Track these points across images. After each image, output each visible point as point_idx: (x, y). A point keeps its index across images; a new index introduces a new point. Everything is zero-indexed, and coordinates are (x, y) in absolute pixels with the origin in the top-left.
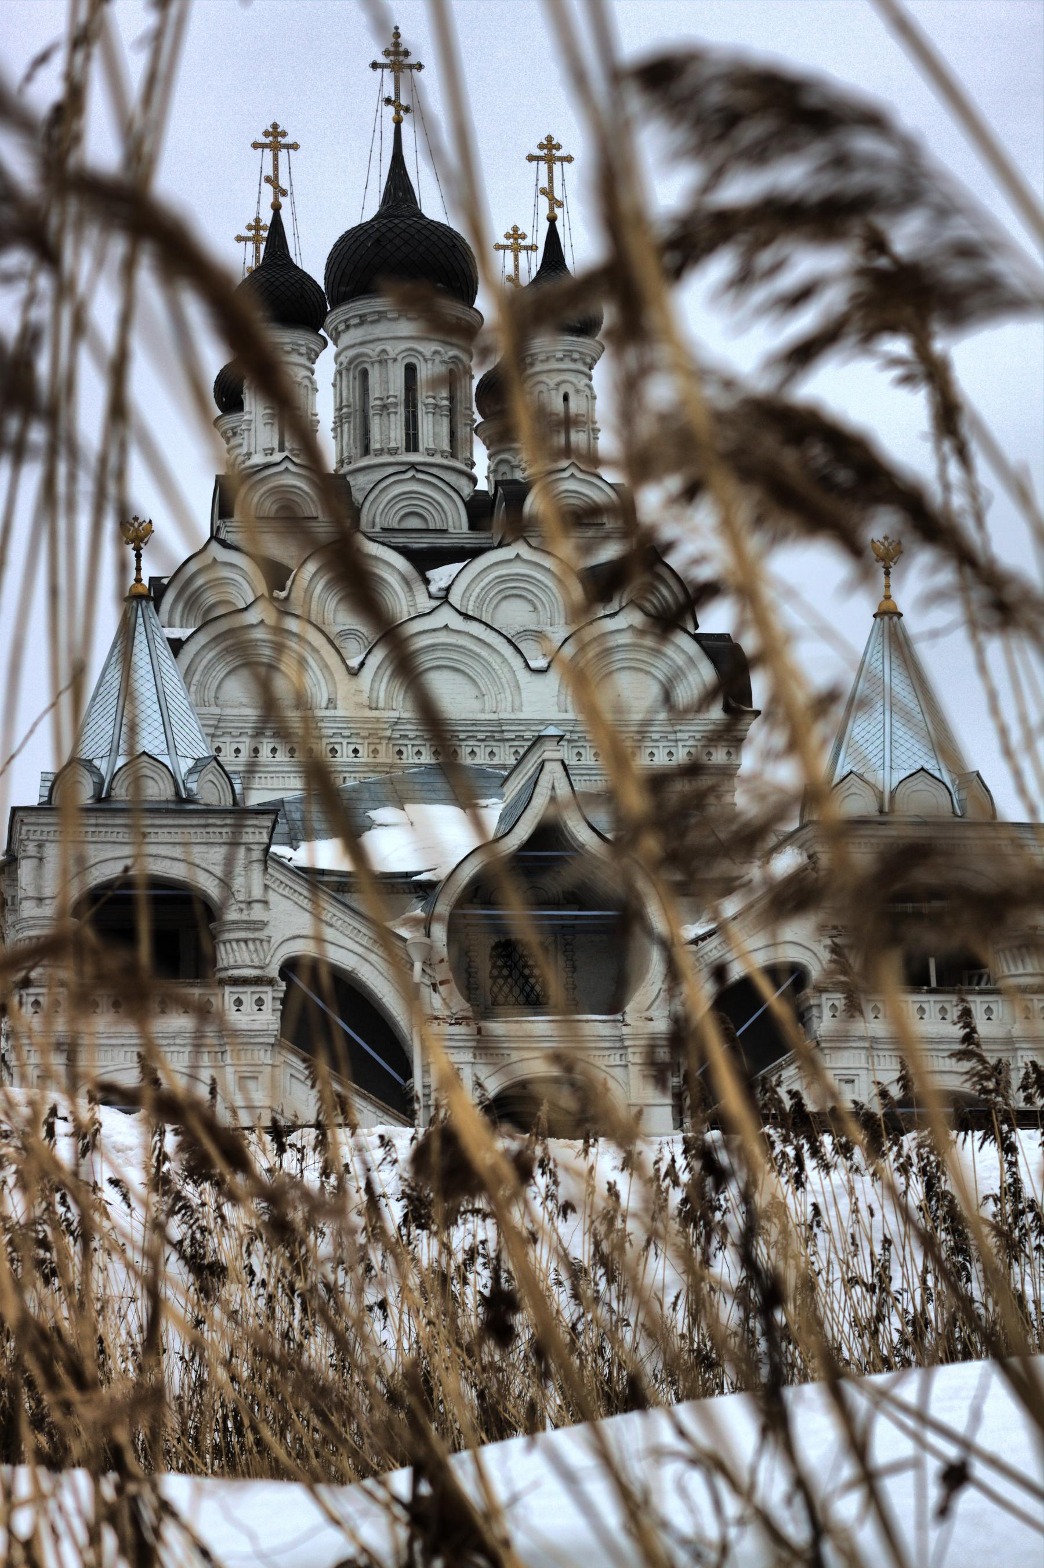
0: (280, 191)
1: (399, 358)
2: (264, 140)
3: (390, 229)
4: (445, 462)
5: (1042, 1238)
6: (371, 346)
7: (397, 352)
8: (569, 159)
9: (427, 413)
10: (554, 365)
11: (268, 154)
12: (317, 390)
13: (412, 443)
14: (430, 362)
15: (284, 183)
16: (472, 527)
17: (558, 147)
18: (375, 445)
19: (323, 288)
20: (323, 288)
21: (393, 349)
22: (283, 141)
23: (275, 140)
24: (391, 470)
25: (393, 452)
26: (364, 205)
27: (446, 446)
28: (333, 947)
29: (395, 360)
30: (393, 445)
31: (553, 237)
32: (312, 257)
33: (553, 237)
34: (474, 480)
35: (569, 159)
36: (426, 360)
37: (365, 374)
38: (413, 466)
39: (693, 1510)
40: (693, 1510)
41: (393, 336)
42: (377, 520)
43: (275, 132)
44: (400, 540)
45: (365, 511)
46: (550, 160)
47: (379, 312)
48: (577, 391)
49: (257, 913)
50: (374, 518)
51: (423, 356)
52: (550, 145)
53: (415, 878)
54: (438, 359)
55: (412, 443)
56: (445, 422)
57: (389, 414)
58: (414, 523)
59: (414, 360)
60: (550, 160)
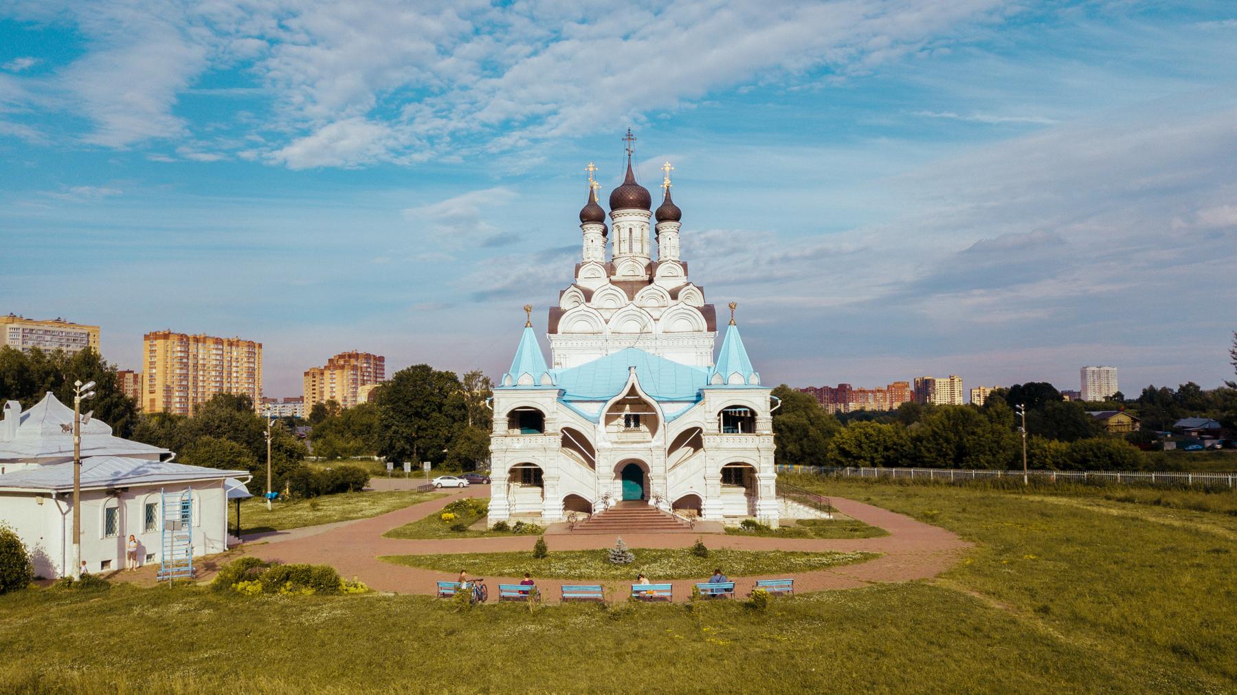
13: (631, 250)
26: (619, 181)
49: (554, 416)
55: (631, 250)
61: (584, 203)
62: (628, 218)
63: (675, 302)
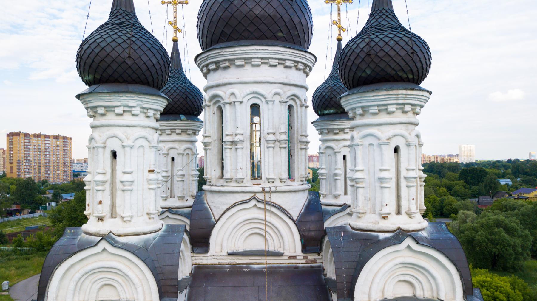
0: (177, 30)
1: (245, 100)
3: (125, 41)
5: (444, 281)
6: (223, 88)
7: (243, 95)
9: (268, 147)
10: (383, 118)
11: (171, 7)
13: (256, 171)
14: (270, 103)
15: (179, 25)
16: (305, 250)
18: (227, 175)
19: (170, 55)
20: (170, 55)
21: (240, 92)
24: (240, 198)
25: (240, 181)
27: (285, 175)
29: (241, 102)
30: (239, 176)
36: (267, 102)
37: (220, 109)
42: (225, 244)
45: (218, 226)
47: (229, 60)
48: (408, 145)
50: (222, 241)
51: (265, 98)
54: (277, 99)
55: (256, 171)
56: (284, 154)
57: (237, 149)
58: (257, 244)
59: (257, 101)
62: (249, 73)
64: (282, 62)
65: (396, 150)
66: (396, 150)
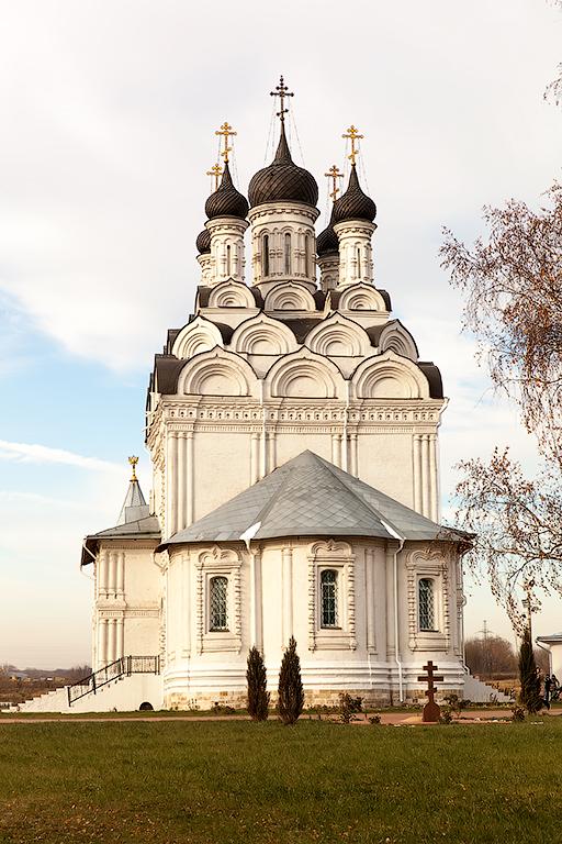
2: (212, 171)
4: (305, 279)
8: (342, 176)
11: (332, 178)
12: (146, 706)
17: (286, 88)
22: (286, 92)
23: (353, 134)
26: (266, 158)
27: (303, 272)
28: (196, 514)
31: (354, 173)
32: (242, 187)
33: (354, 173)
34: (316, 287)
35: (342, 176)
37: (266, 237)
38: (290, 281)
39: (430, 512)
40: (430, 512)
41: (285, 217)
43: (352, 130)
44: (286, 317)
46: (282, 95)
52: (334, 169)
53: (29, 707)
56: (303, 261)
60: (334, 176)
61: (210, 186)
63: (375, 351)
64: (301, 213)
65: (229, 247)
66: (229, 247)
